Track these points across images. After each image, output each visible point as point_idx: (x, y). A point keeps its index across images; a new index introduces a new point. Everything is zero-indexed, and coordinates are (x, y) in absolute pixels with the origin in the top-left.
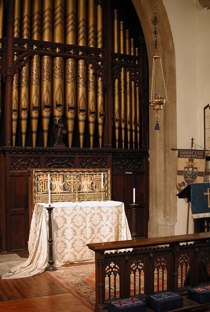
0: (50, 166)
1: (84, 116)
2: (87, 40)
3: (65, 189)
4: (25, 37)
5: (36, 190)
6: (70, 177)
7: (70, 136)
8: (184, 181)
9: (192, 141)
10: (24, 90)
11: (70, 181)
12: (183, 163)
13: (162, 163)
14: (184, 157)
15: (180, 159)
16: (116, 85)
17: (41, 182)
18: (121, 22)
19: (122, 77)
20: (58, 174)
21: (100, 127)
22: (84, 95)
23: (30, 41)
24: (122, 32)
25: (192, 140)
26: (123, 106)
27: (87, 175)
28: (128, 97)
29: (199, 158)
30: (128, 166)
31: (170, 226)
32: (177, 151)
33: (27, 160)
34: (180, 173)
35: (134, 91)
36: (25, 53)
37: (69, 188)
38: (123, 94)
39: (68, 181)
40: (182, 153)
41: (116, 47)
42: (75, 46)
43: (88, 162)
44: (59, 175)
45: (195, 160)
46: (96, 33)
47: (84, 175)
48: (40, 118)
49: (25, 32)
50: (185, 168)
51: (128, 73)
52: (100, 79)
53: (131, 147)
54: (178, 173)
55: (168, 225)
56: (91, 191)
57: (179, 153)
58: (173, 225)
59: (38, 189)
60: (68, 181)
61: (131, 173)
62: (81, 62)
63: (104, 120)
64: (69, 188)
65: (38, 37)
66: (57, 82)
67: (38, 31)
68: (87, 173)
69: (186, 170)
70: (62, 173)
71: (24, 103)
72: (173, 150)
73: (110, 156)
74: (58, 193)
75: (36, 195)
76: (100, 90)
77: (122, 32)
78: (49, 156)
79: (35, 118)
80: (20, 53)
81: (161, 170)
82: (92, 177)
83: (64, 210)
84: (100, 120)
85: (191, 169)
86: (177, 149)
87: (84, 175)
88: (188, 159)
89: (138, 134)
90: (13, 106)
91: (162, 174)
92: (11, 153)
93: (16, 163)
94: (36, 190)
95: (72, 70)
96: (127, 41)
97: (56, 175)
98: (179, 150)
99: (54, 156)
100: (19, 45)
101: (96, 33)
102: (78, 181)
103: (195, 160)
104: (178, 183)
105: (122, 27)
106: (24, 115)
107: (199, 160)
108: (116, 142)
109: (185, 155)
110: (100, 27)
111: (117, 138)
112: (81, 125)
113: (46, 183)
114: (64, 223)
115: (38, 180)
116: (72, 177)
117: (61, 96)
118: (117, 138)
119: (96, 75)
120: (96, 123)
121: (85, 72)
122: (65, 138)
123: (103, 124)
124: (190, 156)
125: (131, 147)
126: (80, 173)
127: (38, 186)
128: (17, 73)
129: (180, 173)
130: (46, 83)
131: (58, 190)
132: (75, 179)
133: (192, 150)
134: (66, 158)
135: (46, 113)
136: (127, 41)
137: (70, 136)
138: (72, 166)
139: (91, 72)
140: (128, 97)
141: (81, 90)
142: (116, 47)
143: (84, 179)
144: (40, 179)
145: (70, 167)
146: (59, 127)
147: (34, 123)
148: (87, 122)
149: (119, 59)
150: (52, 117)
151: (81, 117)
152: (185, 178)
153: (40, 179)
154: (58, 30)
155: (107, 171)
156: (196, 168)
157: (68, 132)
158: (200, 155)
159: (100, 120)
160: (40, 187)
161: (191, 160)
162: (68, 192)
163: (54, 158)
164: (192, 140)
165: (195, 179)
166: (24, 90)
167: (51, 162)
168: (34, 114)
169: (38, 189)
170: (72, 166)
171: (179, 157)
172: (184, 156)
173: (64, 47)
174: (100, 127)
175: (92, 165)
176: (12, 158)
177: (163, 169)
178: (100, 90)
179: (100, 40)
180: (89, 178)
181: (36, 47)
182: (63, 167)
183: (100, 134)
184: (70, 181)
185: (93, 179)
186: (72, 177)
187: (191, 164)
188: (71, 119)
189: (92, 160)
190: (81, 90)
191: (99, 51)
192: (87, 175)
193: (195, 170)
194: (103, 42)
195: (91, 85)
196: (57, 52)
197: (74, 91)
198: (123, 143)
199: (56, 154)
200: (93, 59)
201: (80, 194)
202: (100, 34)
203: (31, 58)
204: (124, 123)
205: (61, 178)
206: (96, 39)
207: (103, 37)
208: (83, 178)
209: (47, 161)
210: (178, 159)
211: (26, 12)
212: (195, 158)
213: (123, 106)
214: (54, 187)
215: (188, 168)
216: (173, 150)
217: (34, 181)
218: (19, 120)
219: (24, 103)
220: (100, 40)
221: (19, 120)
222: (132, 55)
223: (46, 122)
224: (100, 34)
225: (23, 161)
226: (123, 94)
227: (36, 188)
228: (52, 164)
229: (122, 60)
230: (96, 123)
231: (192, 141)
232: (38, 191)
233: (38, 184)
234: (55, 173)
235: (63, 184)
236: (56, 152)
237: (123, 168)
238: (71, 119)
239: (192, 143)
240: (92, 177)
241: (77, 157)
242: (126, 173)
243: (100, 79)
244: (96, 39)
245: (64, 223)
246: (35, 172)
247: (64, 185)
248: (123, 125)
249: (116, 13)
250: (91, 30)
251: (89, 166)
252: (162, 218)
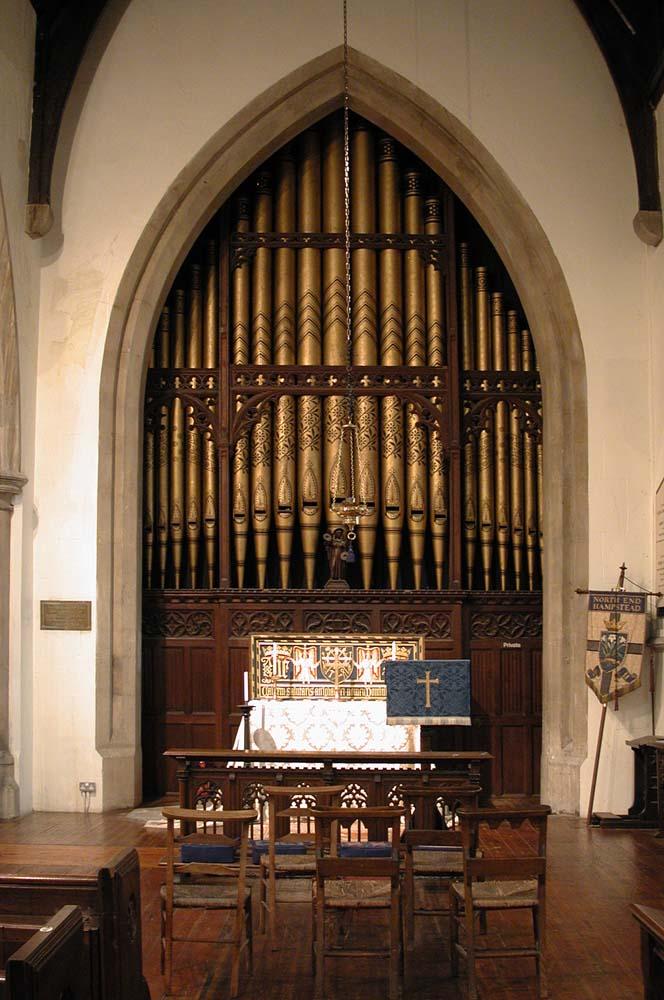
0: (314, 629)
1: (421, 524)
2: (403, 352)
3: (320, 676)
4: (414, 363)
5: (259, 674)
6: (332, 651)
7: (367, 564)
8: (598, 664)
9: (623, 573)
10: (260, 472)
11: (332, 658)
12: (598, 621)
13: (559, 623)
14: (601, 610)
15: (594, 613)
16: (484, 445)
17: (269, 659)
18: (496, 295)
19: (499, 425)
20: (305, 644)
21: (438, 544)
22: (396, 475)
23: (272, 370)
24: (497, 319)
25: (623, 568)
26: (501, 493)
27: (371, 647)
28: (515, 470)
29: (631, 612)
30: (511, 629)
31: (571, 766)
32: (588, 596)
33: (265, 616)
34: (592, 645)
35: (488, 451)
36: (259, 395)
37: (330, 672)
38: (500, 465)
39: (327, 658)
40: (598, 600)
41: (482, 356)
42: (322, 370)
43: (403, 620)
44: (308, 646)
45: (624, 617)
46: (425, 332)
47: (365, 647)
48: (297, 529)
49: (260, 349)
50: (603, 634)
51: (514, 414)
52: (435, 435)
53: (495, 583)
54: (588, 646)
55: (566, 765)
56: (316, 680)
57: (591, 599)
58: (576, 764)
59: (262, 674)
60: (327, 658)
61: (519, 646)
62: (389, 402)
63: (447, 527)
64: (330, 672)
65: (288, 358)
66: (335, 449)
67: (288, 345)
68: (370, 643)
69: (604, 638)
70: (313, 643)
71: (260, 499)
72: (579, 592)
73: (457, 608)
74: (306, 683)
75: (259, 685)
76: (436, 461)
77: (497, 319)
78: (314, 607)
79: (285, 529)
80: (250, 396)
81: (557, 640)
82: (383, 651)
83: (287, 714)
84: (437, 528)
85: (612, 638)
86: (590, 589)
87: (365, 647)
88: (608, 614)
89: (150, 551)
90: (237, 506)
91: (559, 649)
92: (229, 602)
93: (444, 624)
94: (259, 674)
95: (368, 420)
96: (512, 337)
97: (302, 646)
98: (592, 592)
99: (325, 607)
100: (247, 379)
101: (425, 332)
102: (350, 659)
103: (624, 617)
104: (587, 669)
105: (497, 307)
106: (261, 523)
107: (631, 615)
108: (515, 578)
109: (604, 604)
110: (434, 315)
111: (517, 569)
112: (416, 543)
113: (279, 662)
114: (289, 739)
115: (262, 655)
116: (337, 650)
117: (370, 481)
118: (517, 569)
119: (425, 429)
120: (428, 535)
121: (397, 423)
122: (352, 573)
123: (446, 537)
124: (614, 605)
125: (511, 584)
126: (356, 643)
127: (262, 667)
128: (242, 437)
129: (592, 645)
130: (308, 455)
131: (306, 676)
132: (342, 656)
133: (621, 592)
134: (351, 612)
135: (309, 517)
136: (512, 337)
137: (367, 564)
138: (364, 629)
139: (414, 420)
140: (515, 470)
141: (391, 463)
142: (482, 356)
143: (301, 654)
144: (266, 654)
145: (362, 630)
146: (336, 547)
147: (284, 540)
148: (405, 533)
149: (505, 385)
150: (323, 525)
151: (416, 525)
152: (602, 657)
153: (266, 654)
154: (334, 335)
155: (417, 640)
156: (625, 636)
157: (358, 555)
158: (634, 605)
159: (437, 528)
160: (267, 669)
161: (616, 617)
162: (328, 681)
163: (324, 612)
164: (623, 568)
165: (621, 660)
166: (260, 472)
167: (318, 619)
168: (284, 520)
169: (262, 674)
170: (364, 629)
171: (591, 608)
172: (602, 607)
173: (377, 371)
174: (438, 544)
175: (413, 626)
176: (232, 611)
177: (560, 636)
178: (436, 461)
179: (435, 344)
180: (375, 653)
181: (335, 381)
182: (345, 631)
183: (439, 558)
184: (332, 658)
185: (384, 655)
186: (337, 650)
187: (614, 626)
188: (394, 531)
189: (414, 617)
190: (391, 463)
191: (434, 372)
192: (371, 647)
193: (623, 640)
194: (444, 354)
195: (414, 450)
196: (436, 385)
197: (371, 466)
198: (518, 580)
199: (327, 602)
200: (415, 392)
201: (356, 686)
202: (434, 331)
203: (274, 405)
204: (519, 533)
205: (312, 654)
206: (425, 345)
207: (444, 340)
208: (361, 653)
209: (309, 617)
210: (590, 613)
211: (260, 306)
212: (624, 611)
213: (501, 493)
214: (298, 671)
215: (607, 635)
216: (579, 592)
217: (253, 657)
218: (251, 534)
219: (260, 499)
220: (435, 344)
221: (251, 534)
222: (526, 369)
223: (309, 537)
224: (434, 331)
225: (311, 620)
226: (500, 465)
227: (259, 671)
228: (320, 624)
229: (164, 383)
230: (428, 535)
231: (623, 573)
232: (262, 677)
233: (262, 663)
234: (298, 642)
235: (317, 664)
236: (328, 599)
237: (497, 634)
238: (394, 531)
239: (622, 577)
240: (383, 651)
241: (376, 608)
242: (505, 645)
243: (435, 435)
244: (425, 345)
245: (289, 739)
246: (255, 639)
247: (318, 668)
248: (502, 537)
249: (481, 274)
250: (413, 324)
251: (406, 628)
252: (558, 747)
